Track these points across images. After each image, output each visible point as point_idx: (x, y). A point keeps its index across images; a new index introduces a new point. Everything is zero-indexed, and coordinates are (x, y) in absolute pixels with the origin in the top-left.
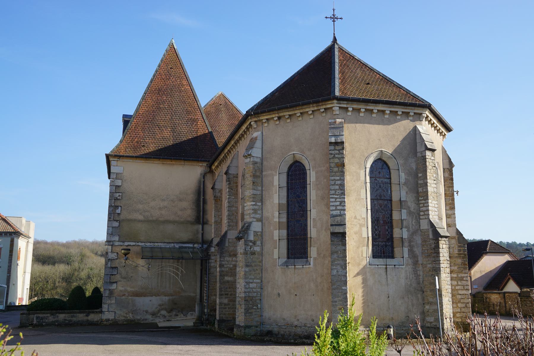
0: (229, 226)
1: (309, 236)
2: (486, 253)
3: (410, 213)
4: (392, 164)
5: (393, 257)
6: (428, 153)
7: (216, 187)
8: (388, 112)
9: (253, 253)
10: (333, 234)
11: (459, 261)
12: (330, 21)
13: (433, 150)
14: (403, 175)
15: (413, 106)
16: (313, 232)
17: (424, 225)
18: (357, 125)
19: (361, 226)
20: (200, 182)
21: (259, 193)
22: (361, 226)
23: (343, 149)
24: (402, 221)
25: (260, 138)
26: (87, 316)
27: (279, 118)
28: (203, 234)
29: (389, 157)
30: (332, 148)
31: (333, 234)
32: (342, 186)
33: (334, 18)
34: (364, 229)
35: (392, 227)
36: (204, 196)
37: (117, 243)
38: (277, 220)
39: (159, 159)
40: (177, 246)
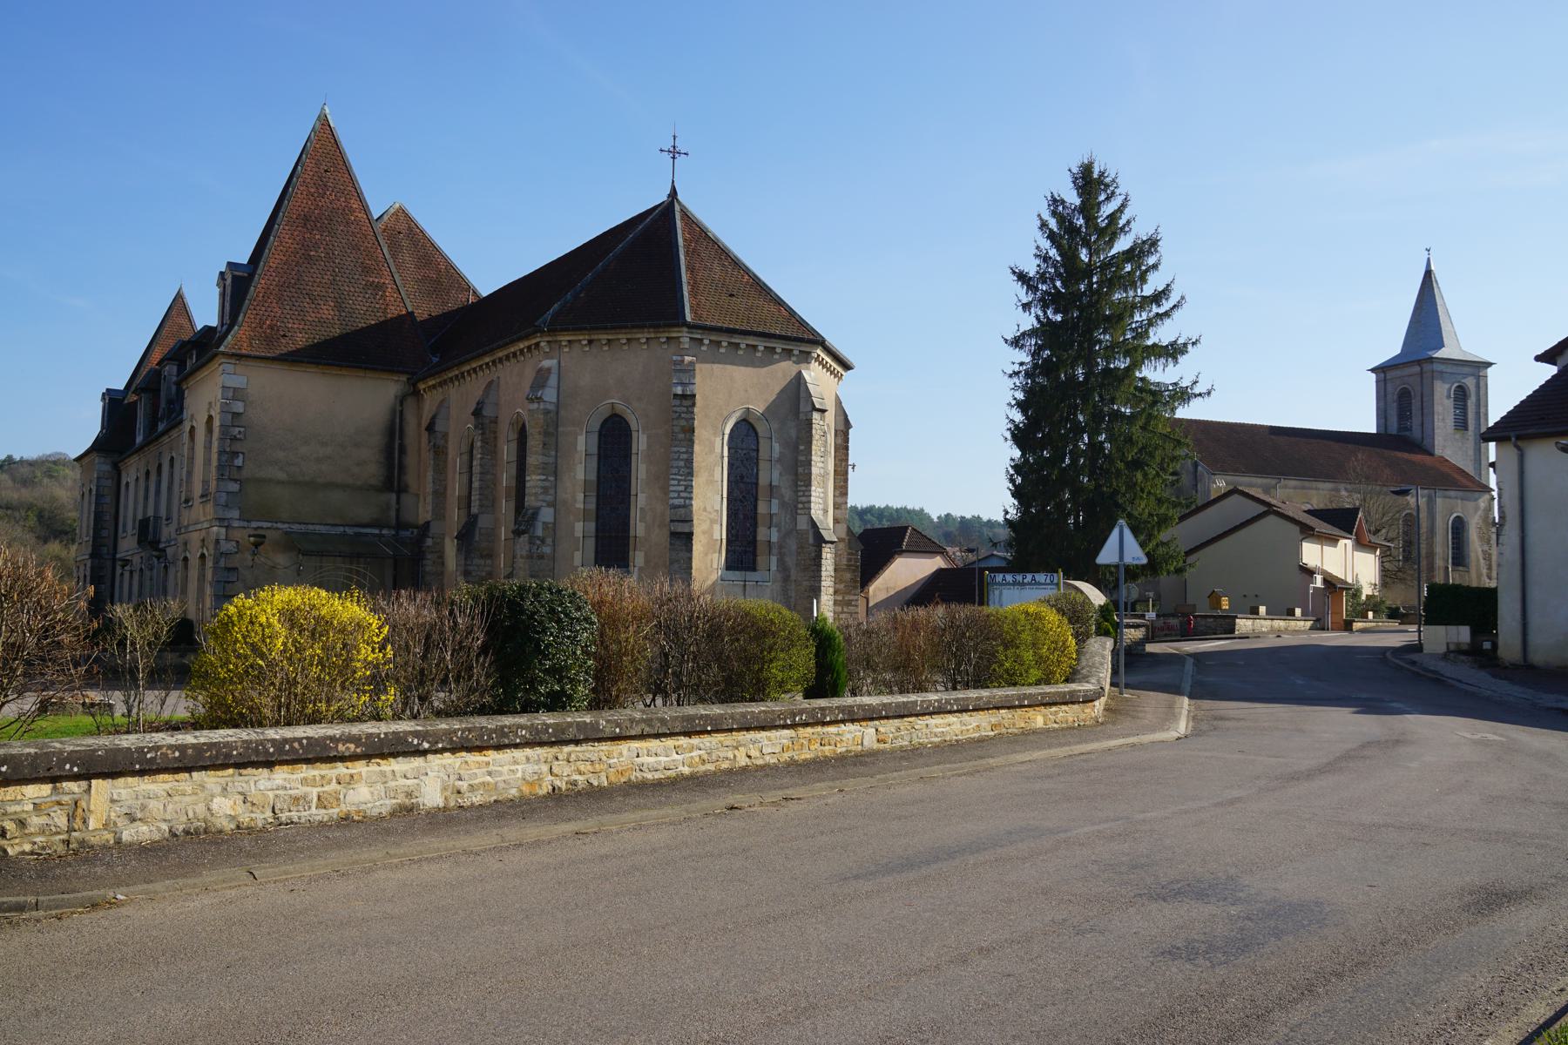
0: (481, 506)
1: (632, 533)
2: (901, 553)
3: (783, 505)
4: (761, 429)
5: (754, 569)
6: (816, 415)
7: (437, 428)
8: (761, 348)
9: (541, 557)
10: (674, 534)
11: (848, 576)
12: (667, 157)
13: (823, 411)
14: (776, 447)
15: (801, 340)
16: (638, 528)
17: (802, 524)
18: (715, 366)
19: (713, 522)
20: (393, 411)
21: (551, 460)
22: (713, 522)
23: (694, 405)
24: (771, 516)
25: (555, 371)
26: (182, 656)
27: (590, 342)
28: (398, 510)
29: (759, 419)
30: (677, 402)
31: (674, 534)
32: (689, 462)
33: (674, 153)
34: (717, 527)
35: (755, 525)
36: (401, 437)
37: (236, 524)
38: (580, 506)
39: (318, 364)
40: (350, 531)
